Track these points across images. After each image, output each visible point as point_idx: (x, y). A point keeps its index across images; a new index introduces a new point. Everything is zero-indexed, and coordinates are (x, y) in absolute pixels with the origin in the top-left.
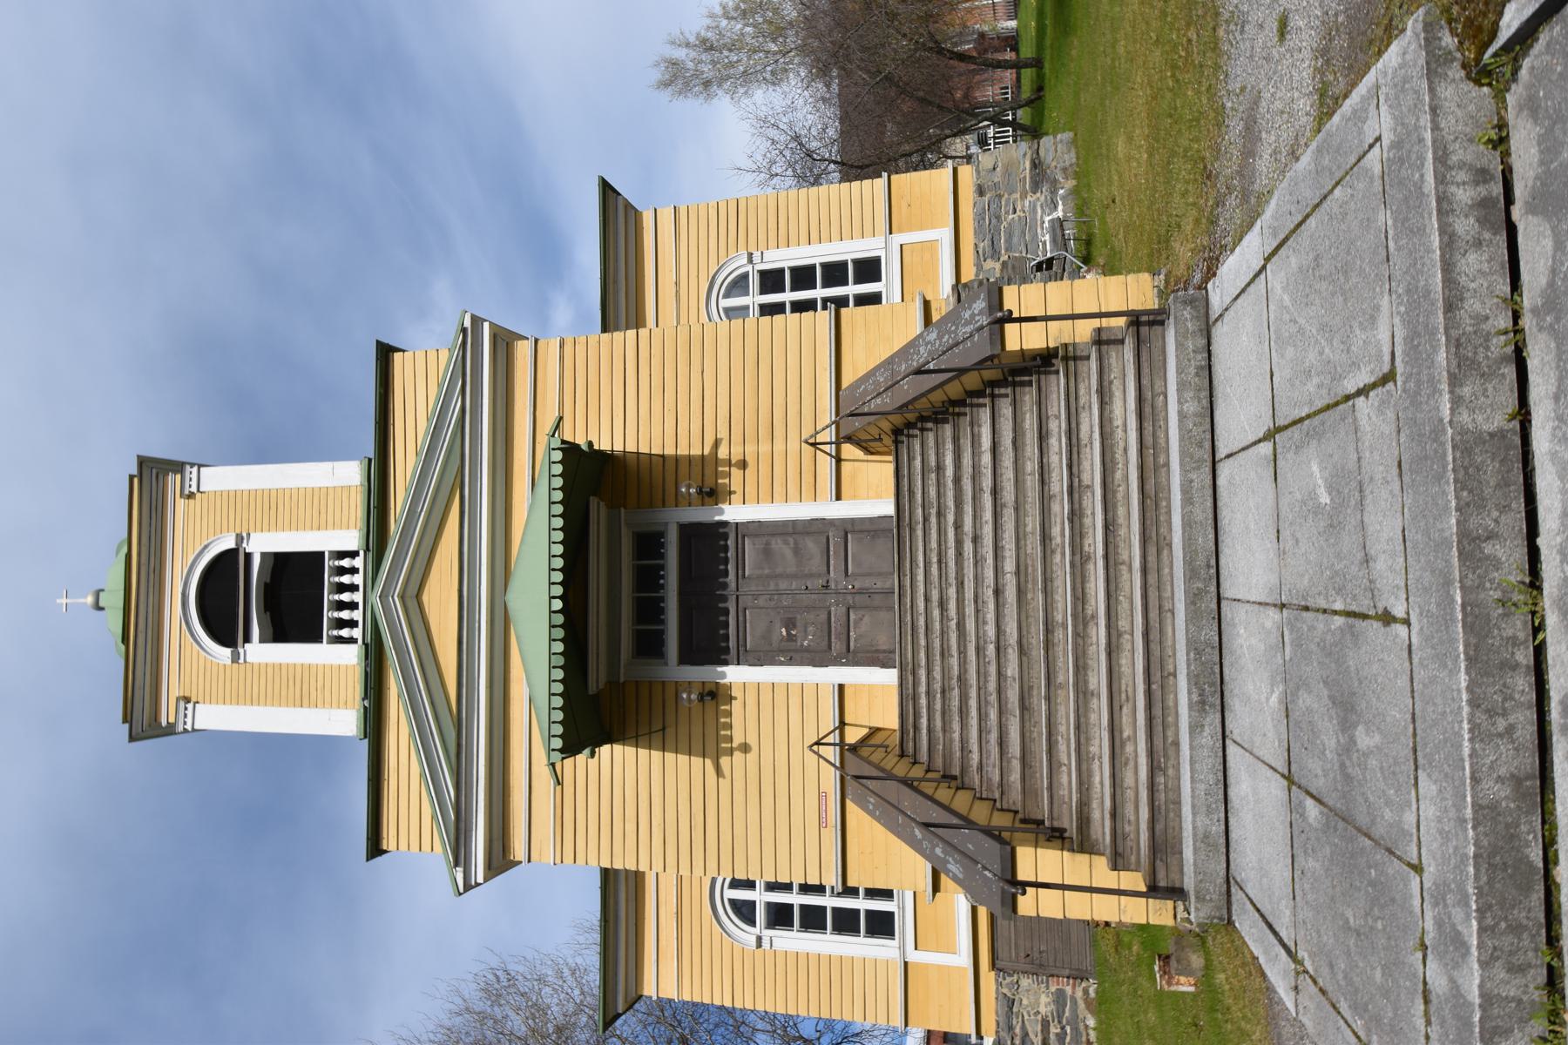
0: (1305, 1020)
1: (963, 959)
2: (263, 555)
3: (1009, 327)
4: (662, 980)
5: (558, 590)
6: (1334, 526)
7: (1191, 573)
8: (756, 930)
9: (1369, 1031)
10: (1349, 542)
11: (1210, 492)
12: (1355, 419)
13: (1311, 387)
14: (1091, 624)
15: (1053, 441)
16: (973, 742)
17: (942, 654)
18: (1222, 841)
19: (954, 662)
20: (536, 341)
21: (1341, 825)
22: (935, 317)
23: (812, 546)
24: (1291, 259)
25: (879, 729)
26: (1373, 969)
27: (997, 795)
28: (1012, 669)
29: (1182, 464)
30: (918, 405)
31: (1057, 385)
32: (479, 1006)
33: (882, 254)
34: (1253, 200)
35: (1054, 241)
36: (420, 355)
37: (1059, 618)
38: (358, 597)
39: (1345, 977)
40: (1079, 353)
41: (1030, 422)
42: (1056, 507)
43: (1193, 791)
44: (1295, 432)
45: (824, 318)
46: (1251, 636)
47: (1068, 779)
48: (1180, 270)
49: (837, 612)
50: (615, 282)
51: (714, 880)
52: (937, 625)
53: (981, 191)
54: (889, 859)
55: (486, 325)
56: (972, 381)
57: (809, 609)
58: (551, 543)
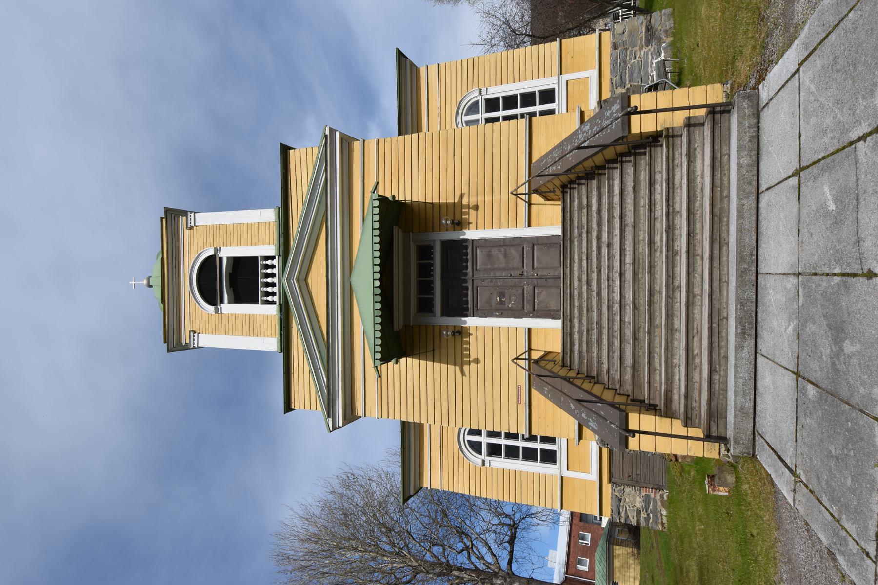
0: (799, 508)
1: (594, 476)
2: (228, 258)
3: (633, 117)
4: (433, 479)
5: (378, 276)
6: (837, 221)
7: (741, 259)
8: (482, 457)
9: (840, 513)
10: (847, 231)
11: (755, 211)
12: (856, 156)
13: (826, 140)
14: (677, 291)
15: (658, 186)
16: (605, 358)
17: (588, 310)
18: (752, 411)
19: (595, 314)
20: (364, 141)
21: (830, 398)
22: (587, 119)
23: (514, 253)
24: (817, 62)
25: (550, 352)
26: (846, 478)
27: (618, 387)
28: (628, 317)
29: (738, 195)
30: (577, 169)
31: (661, 153)
32: (341, 491)
33: (556, 86)
34: (792, 30)
35: (658, 75)
36: (303, 150)
37: (658, 288)
38: (276, 280)
39: (827, 484)
40: (675, 133)
41: (644, 176)
42: (658, 225)
43: (735, 382)
44: (814, 169)
45: (522, 123)
46: (776, 295)
47: (660, 378)
48: (742, 79)
49: (528, 289)
50: (406, 108)
51: (460, 430)
52: (585, 295)
53: (615, 47)
54: (555, 420)
55: (337, 133)
56: (610, 153)
57: (512, 287)
58: (374, 250)
